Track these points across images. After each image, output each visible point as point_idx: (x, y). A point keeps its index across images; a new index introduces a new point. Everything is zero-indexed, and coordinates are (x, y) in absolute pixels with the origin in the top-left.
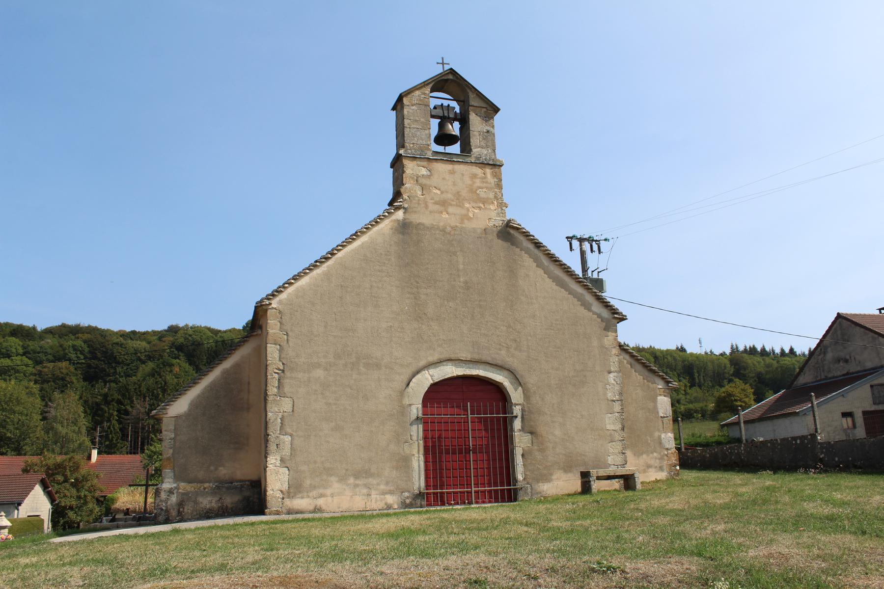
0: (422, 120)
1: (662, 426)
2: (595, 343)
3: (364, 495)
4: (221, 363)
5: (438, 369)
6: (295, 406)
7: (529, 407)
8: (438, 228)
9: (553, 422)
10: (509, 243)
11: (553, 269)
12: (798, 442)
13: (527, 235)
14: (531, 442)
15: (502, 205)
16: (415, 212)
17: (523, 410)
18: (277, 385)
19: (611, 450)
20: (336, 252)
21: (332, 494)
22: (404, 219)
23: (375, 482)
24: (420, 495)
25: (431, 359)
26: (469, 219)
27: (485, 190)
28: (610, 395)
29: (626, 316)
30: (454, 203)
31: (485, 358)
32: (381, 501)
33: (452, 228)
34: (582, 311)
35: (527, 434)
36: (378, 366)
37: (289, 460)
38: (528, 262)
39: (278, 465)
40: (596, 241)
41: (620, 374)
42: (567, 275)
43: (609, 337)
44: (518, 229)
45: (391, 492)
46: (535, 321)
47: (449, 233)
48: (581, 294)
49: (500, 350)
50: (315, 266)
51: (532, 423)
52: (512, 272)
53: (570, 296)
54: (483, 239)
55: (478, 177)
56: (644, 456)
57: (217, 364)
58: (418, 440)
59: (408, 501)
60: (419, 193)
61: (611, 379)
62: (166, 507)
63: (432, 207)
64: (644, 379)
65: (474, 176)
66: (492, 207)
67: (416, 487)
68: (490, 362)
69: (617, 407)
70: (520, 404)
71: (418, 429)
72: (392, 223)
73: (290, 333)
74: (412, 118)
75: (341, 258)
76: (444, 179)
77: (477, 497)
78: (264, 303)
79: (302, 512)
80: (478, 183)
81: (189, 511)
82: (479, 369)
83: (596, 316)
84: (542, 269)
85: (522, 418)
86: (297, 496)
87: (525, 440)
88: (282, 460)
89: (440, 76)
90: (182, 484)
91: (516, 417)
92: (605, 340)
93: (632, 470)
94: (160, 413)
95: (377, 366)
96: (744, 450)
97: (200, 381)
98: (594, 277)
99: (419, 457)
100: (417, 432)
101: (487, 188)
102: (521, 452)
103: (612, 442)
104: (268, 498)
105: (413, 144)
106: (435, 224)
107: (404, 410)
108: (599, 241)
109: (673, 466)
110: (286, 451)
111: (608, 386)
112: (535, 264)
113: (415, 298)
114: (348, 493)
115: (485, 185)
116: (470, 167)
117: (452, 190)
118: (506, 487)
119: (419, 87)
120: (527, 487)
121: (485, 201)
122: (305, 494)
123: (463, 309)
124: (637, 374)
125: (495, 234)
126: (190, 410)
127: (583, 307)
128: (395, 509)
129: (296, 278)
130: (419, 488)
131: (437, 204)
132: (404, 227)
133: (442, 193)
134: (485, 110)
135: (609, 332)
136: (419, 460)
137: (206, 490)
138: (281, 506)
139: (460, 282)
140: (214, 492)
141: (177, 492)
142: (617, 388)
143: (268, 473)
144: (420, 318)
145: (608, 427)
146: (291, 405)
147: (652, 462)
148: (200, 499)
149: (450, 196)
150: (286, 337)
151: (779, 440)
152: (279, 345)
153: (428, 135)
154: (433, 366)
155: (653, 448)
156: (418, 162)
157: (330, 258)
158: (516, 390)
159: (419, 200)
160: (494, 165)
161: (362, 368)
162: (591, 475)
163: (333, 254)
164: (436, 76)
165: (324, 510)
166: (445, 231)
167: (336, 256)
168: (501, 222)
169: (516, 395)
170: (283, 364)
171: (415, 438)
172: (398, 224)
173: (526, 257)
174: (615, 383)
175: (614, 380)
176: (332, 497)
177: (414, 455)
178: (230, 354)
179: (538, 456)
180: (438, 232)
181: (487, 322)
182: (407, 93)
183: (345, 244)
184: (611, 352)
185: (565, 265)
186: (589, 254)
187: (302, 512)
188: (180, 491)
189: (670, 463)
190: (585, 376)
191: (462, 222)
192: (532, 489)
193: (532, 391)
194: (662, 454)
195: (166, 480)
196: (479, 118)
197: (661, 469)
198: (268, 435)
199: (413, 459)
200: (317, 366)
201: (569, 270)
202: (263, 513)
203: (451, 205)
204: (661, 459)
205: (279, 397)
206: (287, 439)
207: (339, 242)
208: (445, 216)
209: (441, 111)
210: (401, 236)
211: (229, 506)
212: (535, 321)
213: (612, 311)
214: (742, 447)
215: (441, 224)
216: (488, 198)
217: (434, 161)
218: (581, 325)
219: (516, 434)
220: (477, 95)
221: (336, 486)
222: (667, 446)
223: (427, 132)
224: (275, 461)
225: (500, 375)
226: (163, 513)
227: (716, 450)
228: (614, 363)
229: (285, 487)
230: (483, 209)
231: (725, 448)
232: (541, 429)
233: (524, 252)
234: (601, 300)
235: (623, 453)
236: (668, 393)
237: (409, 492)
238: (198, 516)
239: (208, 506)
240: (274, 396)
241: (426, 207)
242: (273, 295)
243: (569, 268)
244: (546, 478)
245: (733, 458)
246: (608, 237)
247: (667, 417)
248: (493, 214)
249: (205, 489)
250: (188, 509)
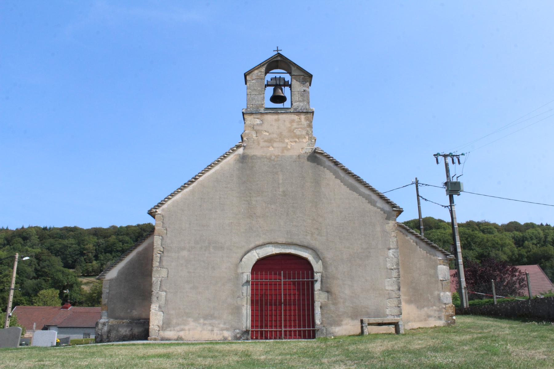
0: (259, 88)
1: (441, 287)
2: (378, 229)
3: (209, 330)
4: (136, 248)
5: (262, 249)
6: (169, 274)
7: (326, 274)
8: (266, 158)
9: (344, 284)
10: (316, 164)
11: (347, 179)
13: (328, 157)
14: (327, 298)
15: (312, 139)
16: (251, 148)
17: (322, 276)
18: (159, 261)
19: (389, 305)
20: (198, 177)
21: (189, 329)
22: (244, 153)
23: (217, 322)
24: (247, 332)
25: (258, 243)
26: (288, 150)
27: (300, 129)
28: (389, 265)
29: (402, 209)
30: (278, 140)
31: (295, 241)
32: (220, 334)
33: (276, 156)
34: (369, 207)
35: (324, 293)
36: (222, 248)
37: (164, 307)
38: (329, 175)
39: (157, 310)
40: (456, 156)
41: (398, 250)
42: (358, 182)
43: (390, 224)
44: (322, 154)
45: (227, 329)
46: (333, 215)
47: (274, 160)
48: (369, 195)
49: (306, 235)
50: (184, 187)
51: (328, 285)
52: (317, 182)
53: (360, 197)
54: (297, 162)
55: (295, 121)
56: (426, 309)
57: (134, 248)
58: (247, 296)
59: (238, 336)
60: (254, 135)
61: (391, 254)
62: (101, 333)
63: (262, 144)
64: (427, 253)
65: (292, 121)
66: (304, 140)
67: (244, 326)
68: (299, 244)
69: (395, 274)
70: (320, 272)
71: (247, 289)
72: (235, 157)
73: (168, 229)
74: (252, 88)
75: (201, 181)
76: (271, 125)
77: (285, 335)
78: (152, 211)
79: (169, 340)
80: (295, 125)
81: (114, 336)
82: (291, 249)
83: (380, 210)
84: (340, 180)
85: (322, 281)
86: (167, 330)
87: (323, 297)
88: (160, 307)
89: (271, 59)
90: (112, 320)
91: (316, 281)
92: (387, 227)
93: (396, 319)
94: (101, 278)
95: (221, 248)
96: (531, 304)
97: (124, 259)
98: (453, 181)
99: (247, 307)
100: (247, 291)
101: (301, 128)
102: (320, 305)
103: (389, 299)
104: (150, 330)
105: (252, 104)
106: (263, 154)
107: (238, 276)
108: (459, 156)
109: (451, 317)
110: (163, 301)
111: (387, 259)
112: (335, 176)
113: (249, 204)
114: (199, 329)
115: (300, 126)
116: (290, 115)
117: (276, 132)
118: (307, 329)
119: (257, 68)
120: (323, 329)
121: (299, 137)
122: (172, 328)
123: (281, 209)
124: (421, 249)
125: (306, 158)
126: (118, 276)
127: (370, 204)
128: (229, 340)
129: (173, 195)
130: (246, 327)
131: (266, 142)
132: (243, 159)
133: (270, 134)
134: (303, 77)
135: (389, 220)
136: (247, 309)
137: (124, 324)
138: (157, 335)
139: (279, 191)
140: (128, 325)
141: (107, 324)
142: (395, 260)
143: (151, 315)
144: (251, 216)
145: (387, 288)
146: (166, 273)
147: (432, 313)
148: (120, 329)
149: (275, 136)
150: (165, 231)
151: (552, 298)
152: (162, 236)
153: (263, 98)
154: (259, 247)
155: (433, 302)
156: (255, 116)
157: (195, 181)
158: (317, 262)
159: (254, 140)
160: (307, 113)
161: (212, 250)
162: (364, 322)
163: (196, 179)
164: (267, 60)
165: (183, 339)
166: (270, 159)
167: (198, 180)
168: (311, 150)
169: (317, 266)
170: (163, 248)
171: (245, 294)
172: (240, 157)
173: (327, 172)
174: (394, 257)
175: (393, 255)
176: (189, 331)
177: (243, 305)
178: (141, 242)
179: (332, 307)
180: (266, 160)
181: (298, 217)
182: (249, 72)
183: (203, 172)
184: (390, 235)
185: (355, 175)
186: (451, 165)
187: (169, 340)
188: (109, 324)
189: (447, 314)
190: (370, 252)
191: (283, 151)
192: (326, 330)
193: (329, 263)
194: (441, 307)
195: (103, 317)
196: (298, 83)
197: (440, 318)
198: (152, 291)
199: (243, 308)
200: (183, 249)
201: (359, 179)
202: (146, 339)
203: (276, 142)
204: (440, 311)
205: (160, 268)
206: (164, 294)
207: (200, 171)
208: (271, 149)
209: (275, 81)
210: (241, 164)
211: (137, 334)
212: (333, 215)
213: (392, 206)
214: (529, 302)
215: (268, 155)
216: (301, 135)
217: (265, 114)
218: (367, 216)
219: (316, 293)
220: (297, 68)
221: (192, 324)
222: (445, 302)
223: (262, 96)
224: (155, 307)
225: (306, 252)
226: (99, 337)
227: (514, 304)
228: (393, 242)
229: (161, 323)
230: (298, 142)
231: (519, 303)
232: (335, 290)
233: (326, 169)
234: (383, 198)
235: (399, 307)
236: (447, 263)
237: (239, 329)
238: (118, 339)
239: (124, 334)
240: (157, 268)
241: (259, 144)
242: (158, 206)
243: (358, 177)
244: (338, 323)
245: (524, 310)
246: (464, 153)
247: (445, 280)
248: (305, 145)
249: (123, 323)
250: (113, 334)
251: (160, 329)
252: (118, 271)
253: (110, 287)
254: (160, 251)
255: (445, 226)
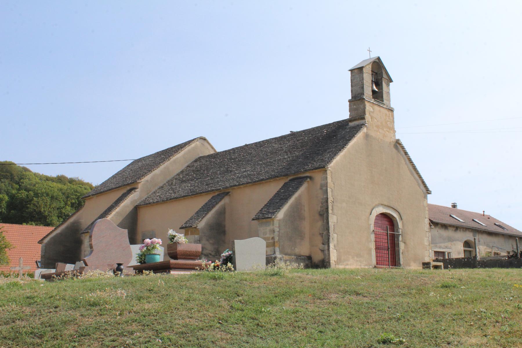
12: (466, 260)
65: (386, 115)
73: (335, 183)
229: (336, 260)
251: (336, 263)
252: (284, 213)
253: (279, 226)
254: (332, 201)
255: (31, 177)
